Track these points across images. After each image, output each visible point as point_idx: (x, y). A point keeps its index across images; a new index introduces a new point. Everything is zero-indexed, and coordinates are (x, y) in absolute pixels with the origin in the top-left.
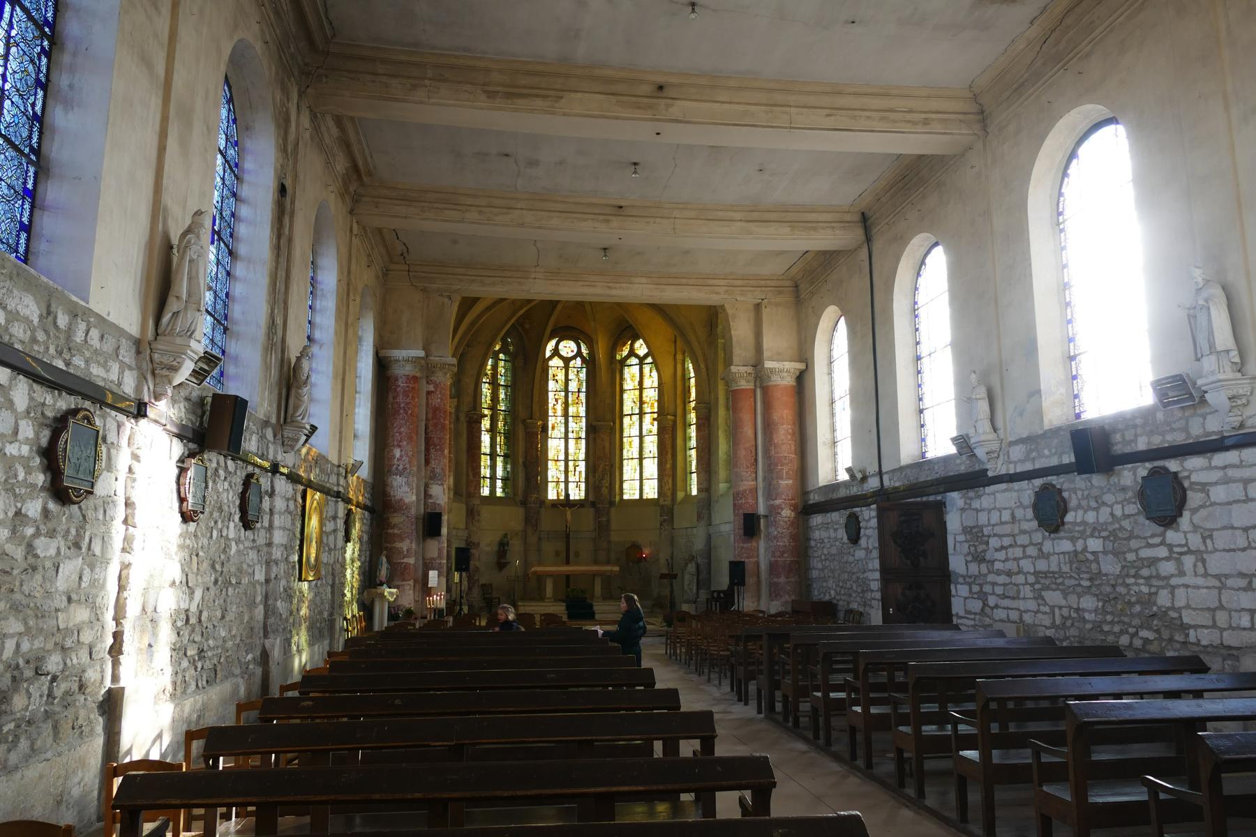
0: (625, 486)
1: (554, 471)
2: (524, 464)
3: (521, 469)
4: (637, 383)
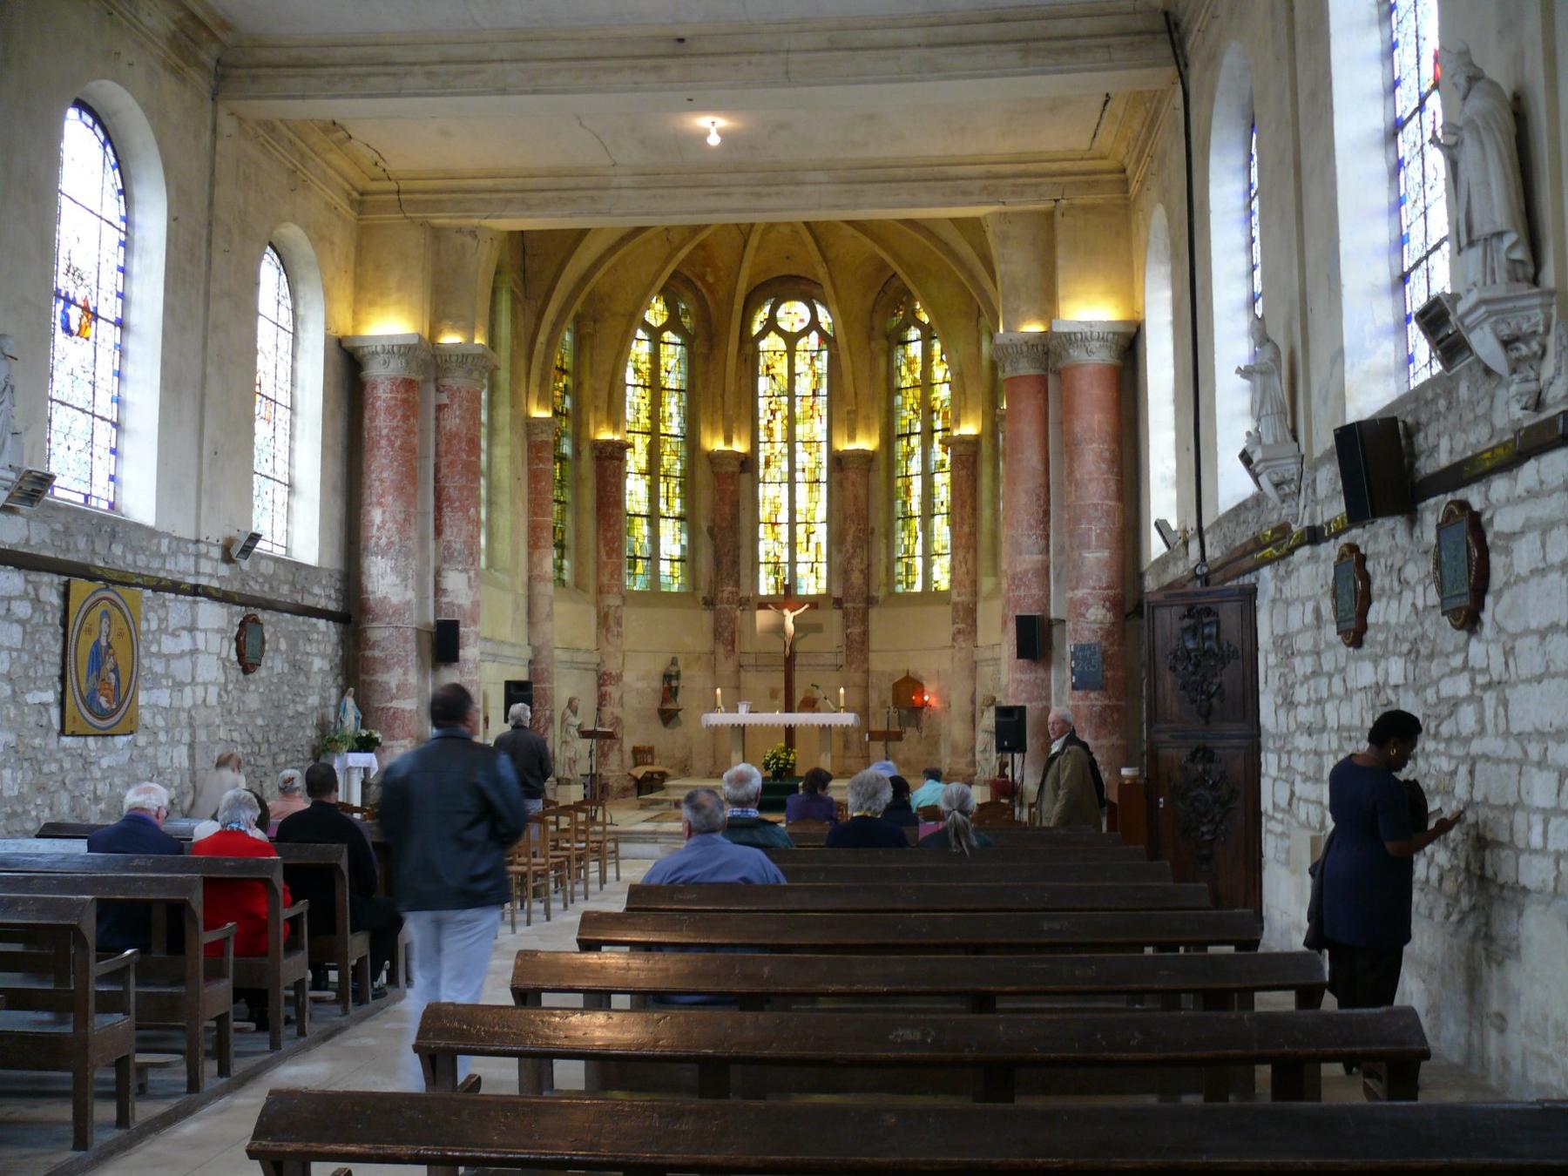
1: (770, 545)
2: (711, 530)
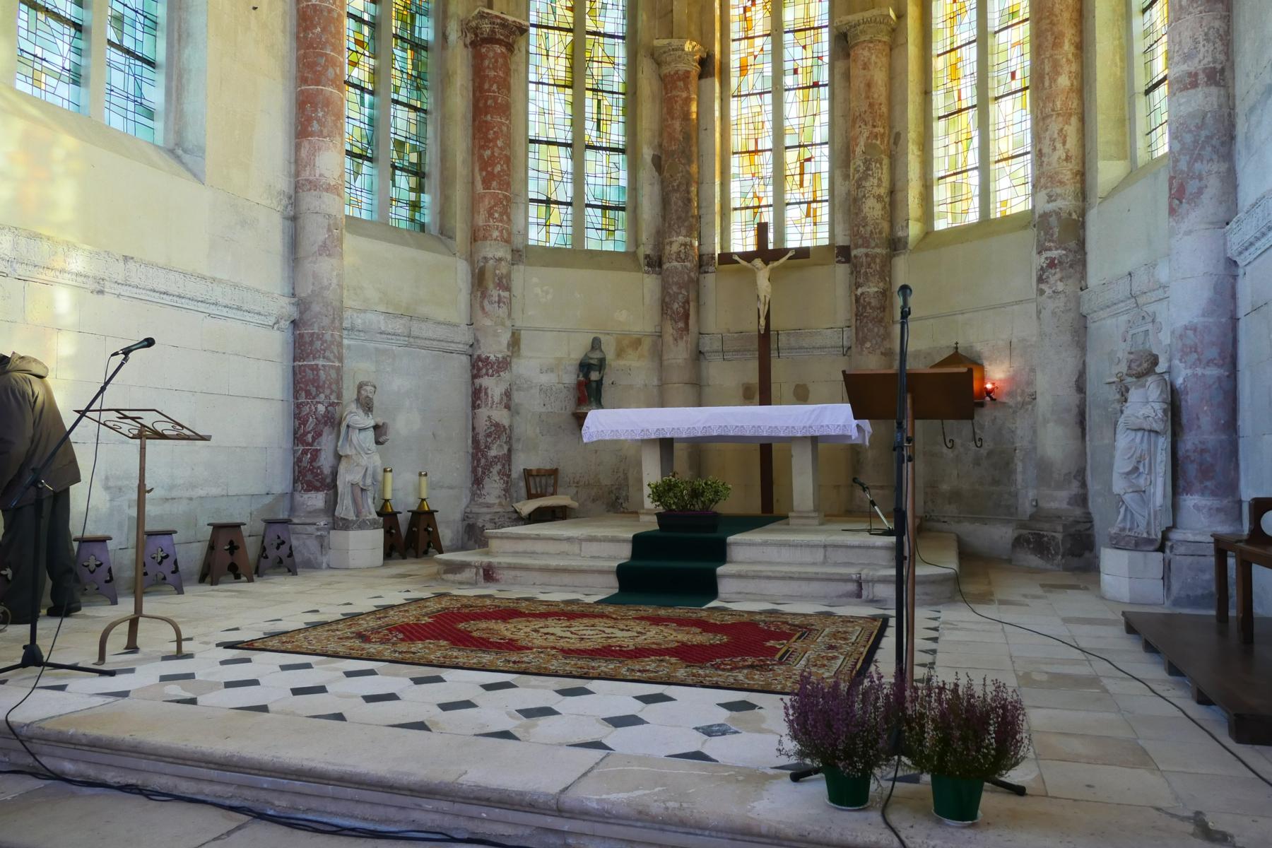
0: (941, 193)
2: (658, 163)
3: (647, 173)
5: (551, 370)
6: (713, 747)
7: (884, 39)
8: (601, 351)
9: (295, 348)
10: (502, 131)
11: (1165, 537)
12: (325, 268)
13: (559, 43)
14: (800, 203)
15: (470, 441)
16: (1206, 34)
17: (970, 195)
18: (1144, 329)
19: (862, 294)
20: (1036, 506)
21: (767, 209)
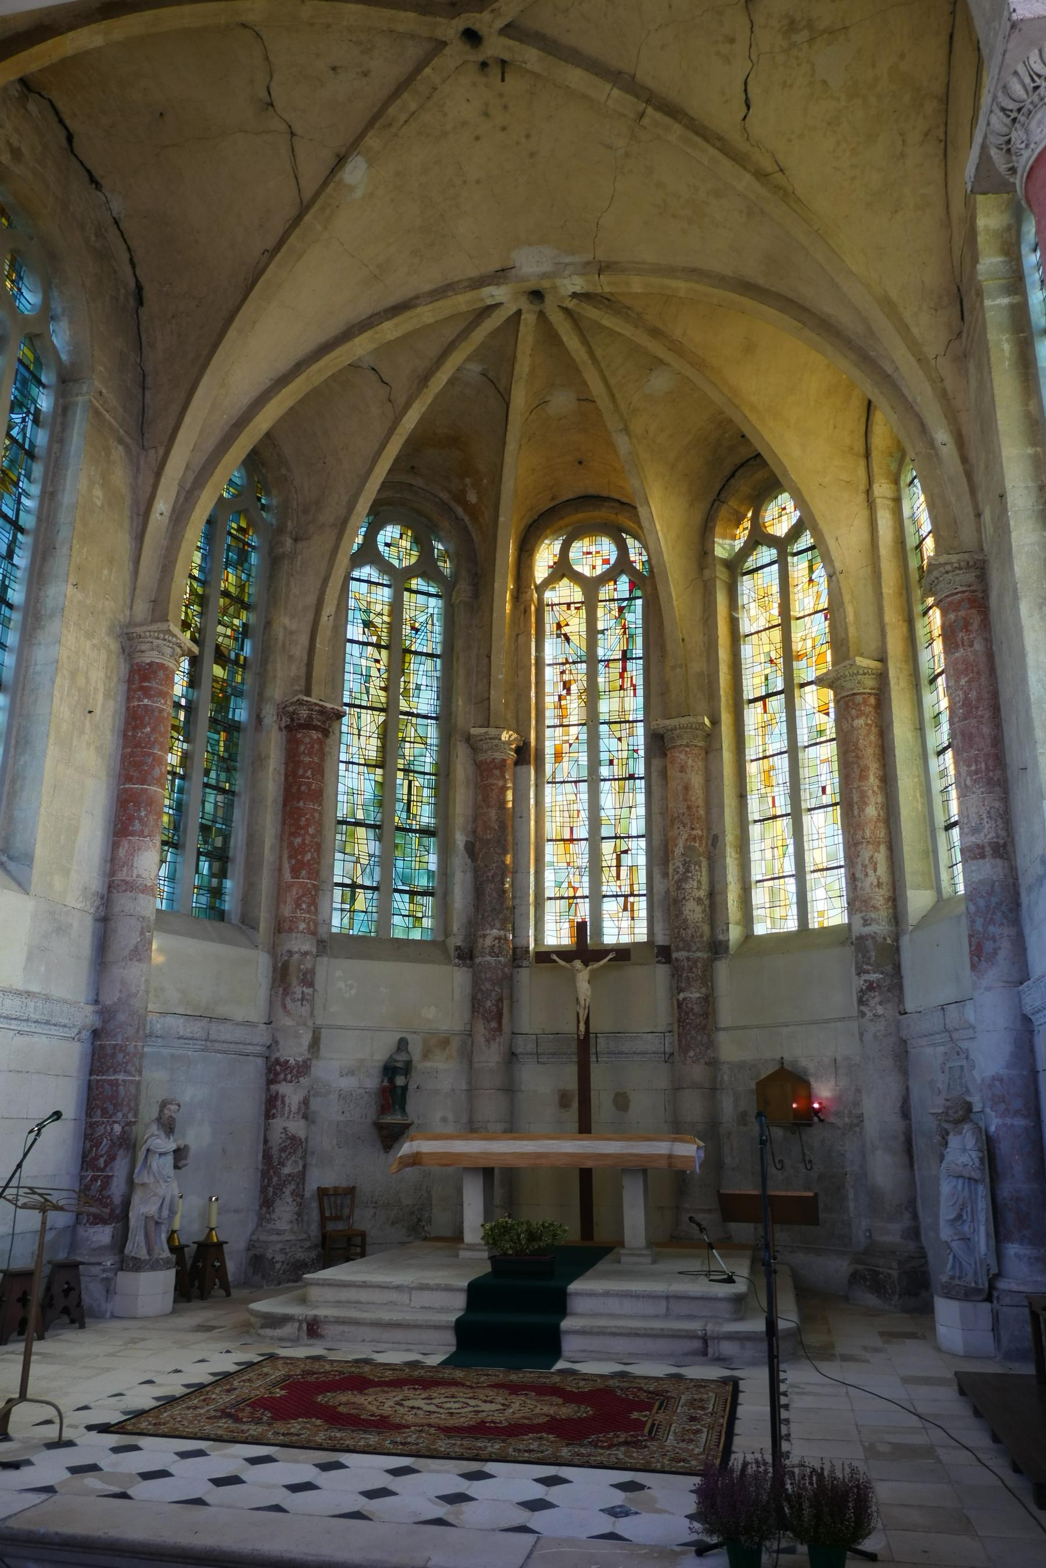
0: (759, 896)
2: (470, 849)
3: (460, 860)
4: (775, 611)
5: (351, 1073)
6: (623, 1526)
7: (700, 744)
8: (408, 1052)
9: (93, 1060)
10: (314, 818)
11: (992, 1287)
12: (133, 973)
13: (371, 722)
14: (617, 896)
15: (260, 1157)
16: (989, 813)
17: (788, 902)
18: (959, 1063)
19: (684, 999)
20: (871, 1236)
21: (582, 900)
